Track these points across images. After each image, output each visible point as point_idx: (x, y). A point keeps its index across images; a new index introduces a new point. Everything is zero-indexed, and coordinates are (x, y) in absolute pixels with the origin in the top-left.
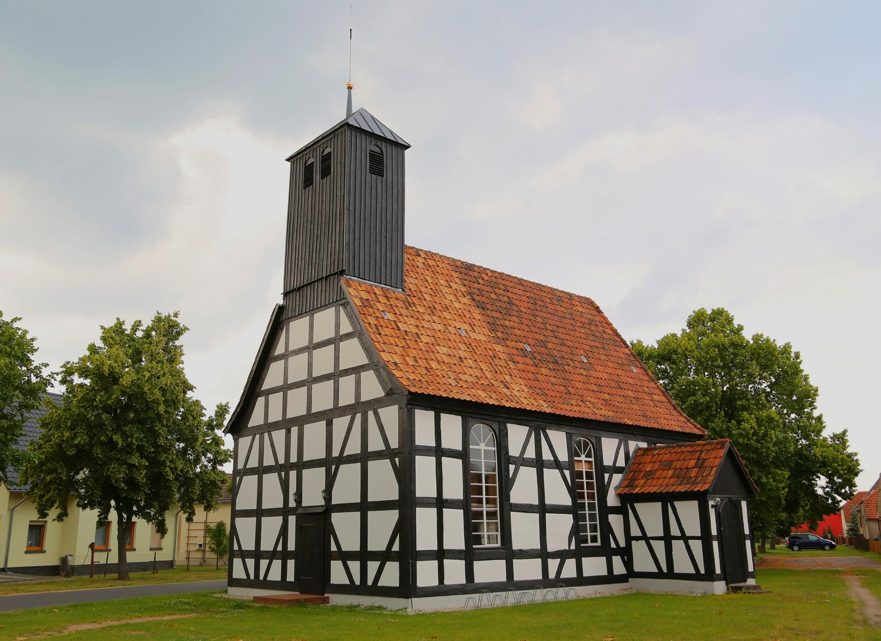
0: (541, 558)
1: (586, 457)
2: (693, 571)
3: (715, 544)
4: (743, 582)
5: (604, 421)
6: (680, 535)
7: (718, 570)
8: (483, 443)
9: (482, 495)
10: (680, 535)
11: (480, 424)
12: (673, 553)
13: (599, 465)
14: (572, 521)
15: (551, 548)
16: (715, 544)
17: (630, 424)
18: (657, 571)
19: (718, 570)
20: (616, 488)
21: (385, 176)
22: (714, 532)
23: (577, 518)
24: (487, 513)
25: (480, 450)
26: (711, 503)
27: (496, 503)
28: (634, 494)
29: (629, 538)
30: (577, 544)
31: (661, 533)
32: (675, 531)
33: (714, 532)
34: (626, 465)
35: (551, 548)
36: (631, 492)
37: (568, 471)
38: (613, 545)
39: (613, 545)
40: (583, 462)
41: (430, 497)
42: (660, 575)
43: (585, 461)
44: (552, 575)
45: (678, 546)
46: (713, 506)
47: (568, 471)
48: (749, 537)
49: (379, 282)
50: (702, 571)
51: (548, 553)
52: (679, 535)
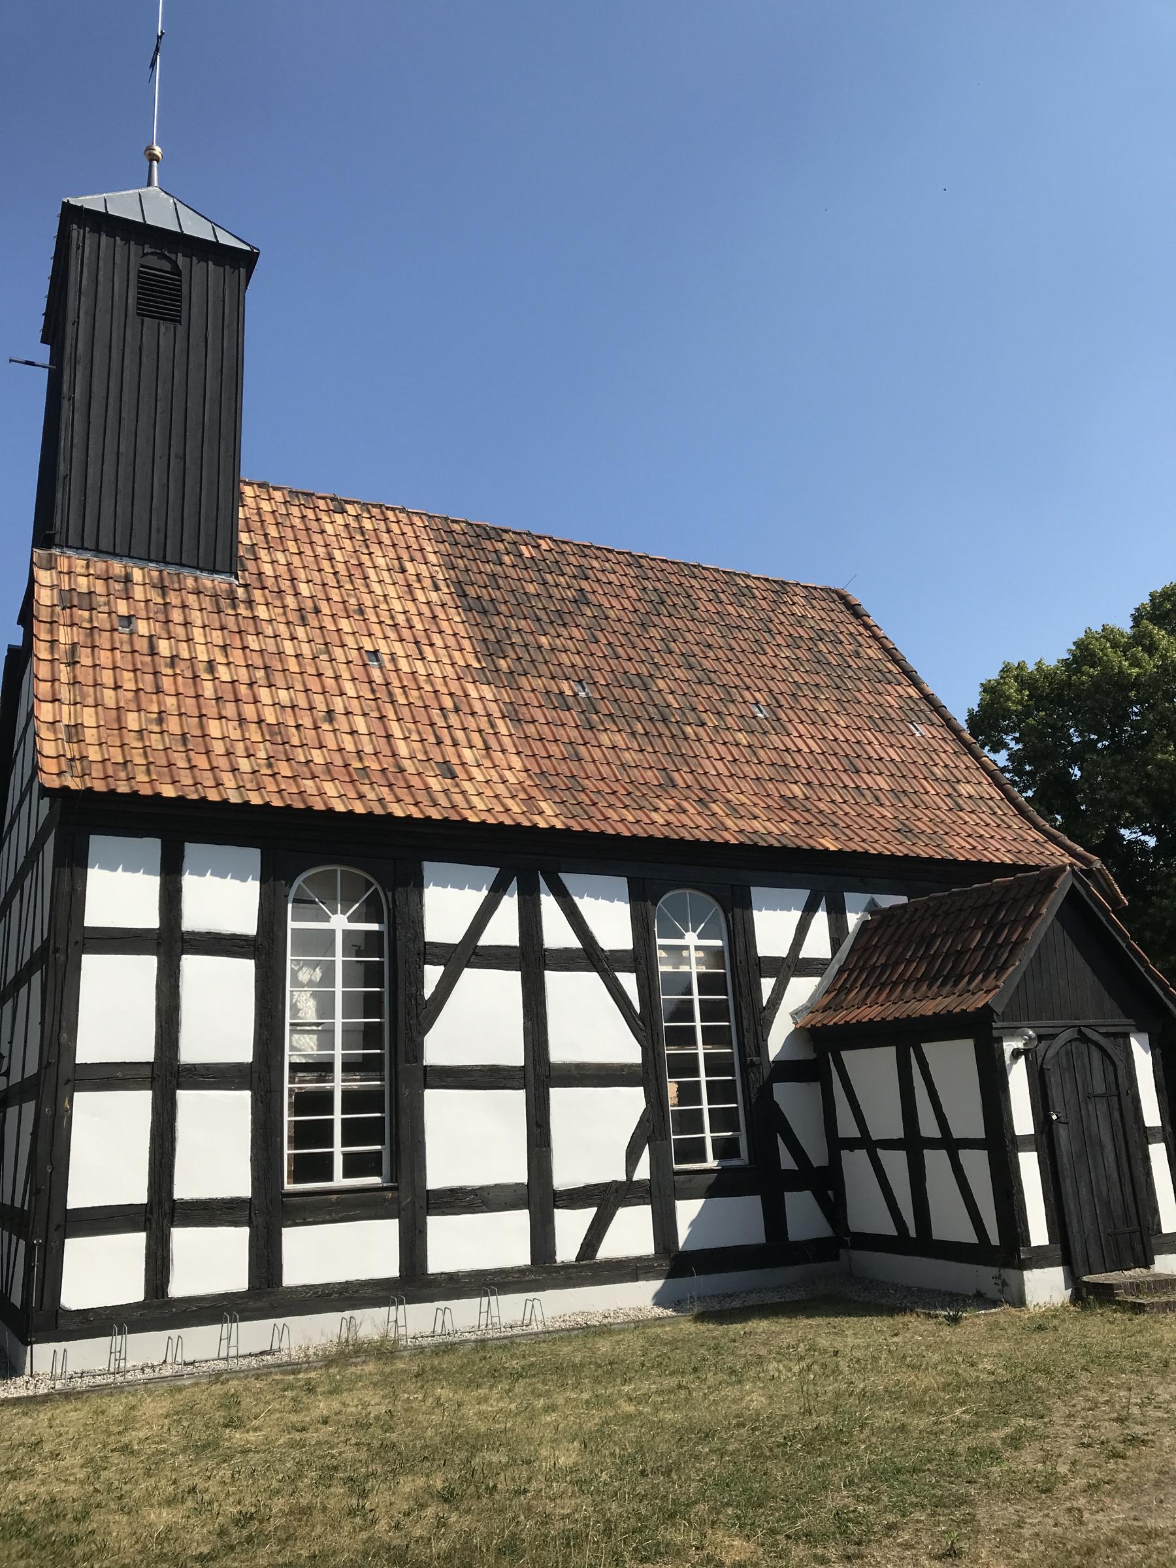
0: (398, 1217)
1: (700, 937)
2: (972, 1238)
3: (1029, 1165)
4: (1138, 1265)
5: (906, 855)
6: (940, 1136)
7: (1039, 1234)
8: (694, 931)
9: (333, 1050)
10: (940, 1136)
11: (682, 891)
12: (927, 1185)
13: (741, 956)
14: (642, 1105)
15: (564, 1178)
16: (1029, 1165)
17: (415, 816)
18: (896, 1234)
19: (1039, 1234)
20: (795, 1015)
21: (184, 319)
22: (1023, 1122)
23: (655, 1099)
24: (346, 1094)
25: (332, 932)
26: (1009, 1046)
27: (381, 1069)
28: (1135, 1021)
29: (836, 1144)
30: (657, 1164)
31: (898, 1133)
32: (929, 1127)
33: (1023, 1122)
34: (834, 954)
35: (564, 1178)
36: (825, 1022)
37: (633, 976)
38: (787, 1161)
39: (787, 1161)
40: (692, 949)
41: (127, 1061)
42: (899, 1244)
43: (697, 948)
44: (567, 1249)
45: (936, 1161)
46: (1016, 1054)
47: (633, 976)
48: (1160, 1136)
49: (144, 555)
50: (995, 1240)
51: (555, 1193)
52: (937, 1134)
